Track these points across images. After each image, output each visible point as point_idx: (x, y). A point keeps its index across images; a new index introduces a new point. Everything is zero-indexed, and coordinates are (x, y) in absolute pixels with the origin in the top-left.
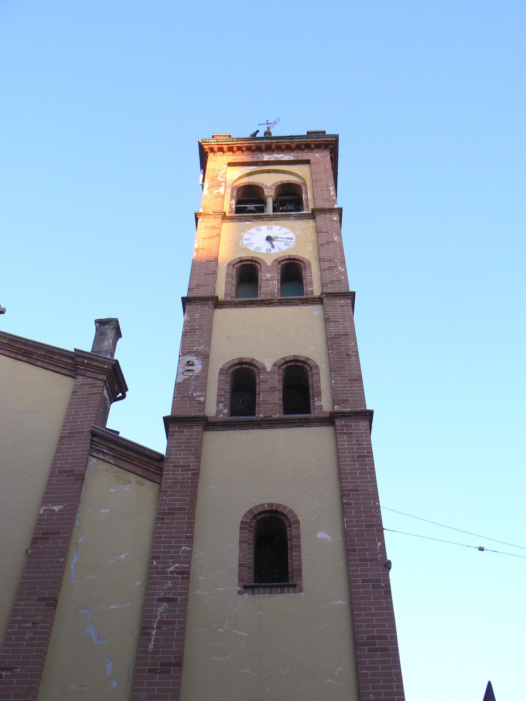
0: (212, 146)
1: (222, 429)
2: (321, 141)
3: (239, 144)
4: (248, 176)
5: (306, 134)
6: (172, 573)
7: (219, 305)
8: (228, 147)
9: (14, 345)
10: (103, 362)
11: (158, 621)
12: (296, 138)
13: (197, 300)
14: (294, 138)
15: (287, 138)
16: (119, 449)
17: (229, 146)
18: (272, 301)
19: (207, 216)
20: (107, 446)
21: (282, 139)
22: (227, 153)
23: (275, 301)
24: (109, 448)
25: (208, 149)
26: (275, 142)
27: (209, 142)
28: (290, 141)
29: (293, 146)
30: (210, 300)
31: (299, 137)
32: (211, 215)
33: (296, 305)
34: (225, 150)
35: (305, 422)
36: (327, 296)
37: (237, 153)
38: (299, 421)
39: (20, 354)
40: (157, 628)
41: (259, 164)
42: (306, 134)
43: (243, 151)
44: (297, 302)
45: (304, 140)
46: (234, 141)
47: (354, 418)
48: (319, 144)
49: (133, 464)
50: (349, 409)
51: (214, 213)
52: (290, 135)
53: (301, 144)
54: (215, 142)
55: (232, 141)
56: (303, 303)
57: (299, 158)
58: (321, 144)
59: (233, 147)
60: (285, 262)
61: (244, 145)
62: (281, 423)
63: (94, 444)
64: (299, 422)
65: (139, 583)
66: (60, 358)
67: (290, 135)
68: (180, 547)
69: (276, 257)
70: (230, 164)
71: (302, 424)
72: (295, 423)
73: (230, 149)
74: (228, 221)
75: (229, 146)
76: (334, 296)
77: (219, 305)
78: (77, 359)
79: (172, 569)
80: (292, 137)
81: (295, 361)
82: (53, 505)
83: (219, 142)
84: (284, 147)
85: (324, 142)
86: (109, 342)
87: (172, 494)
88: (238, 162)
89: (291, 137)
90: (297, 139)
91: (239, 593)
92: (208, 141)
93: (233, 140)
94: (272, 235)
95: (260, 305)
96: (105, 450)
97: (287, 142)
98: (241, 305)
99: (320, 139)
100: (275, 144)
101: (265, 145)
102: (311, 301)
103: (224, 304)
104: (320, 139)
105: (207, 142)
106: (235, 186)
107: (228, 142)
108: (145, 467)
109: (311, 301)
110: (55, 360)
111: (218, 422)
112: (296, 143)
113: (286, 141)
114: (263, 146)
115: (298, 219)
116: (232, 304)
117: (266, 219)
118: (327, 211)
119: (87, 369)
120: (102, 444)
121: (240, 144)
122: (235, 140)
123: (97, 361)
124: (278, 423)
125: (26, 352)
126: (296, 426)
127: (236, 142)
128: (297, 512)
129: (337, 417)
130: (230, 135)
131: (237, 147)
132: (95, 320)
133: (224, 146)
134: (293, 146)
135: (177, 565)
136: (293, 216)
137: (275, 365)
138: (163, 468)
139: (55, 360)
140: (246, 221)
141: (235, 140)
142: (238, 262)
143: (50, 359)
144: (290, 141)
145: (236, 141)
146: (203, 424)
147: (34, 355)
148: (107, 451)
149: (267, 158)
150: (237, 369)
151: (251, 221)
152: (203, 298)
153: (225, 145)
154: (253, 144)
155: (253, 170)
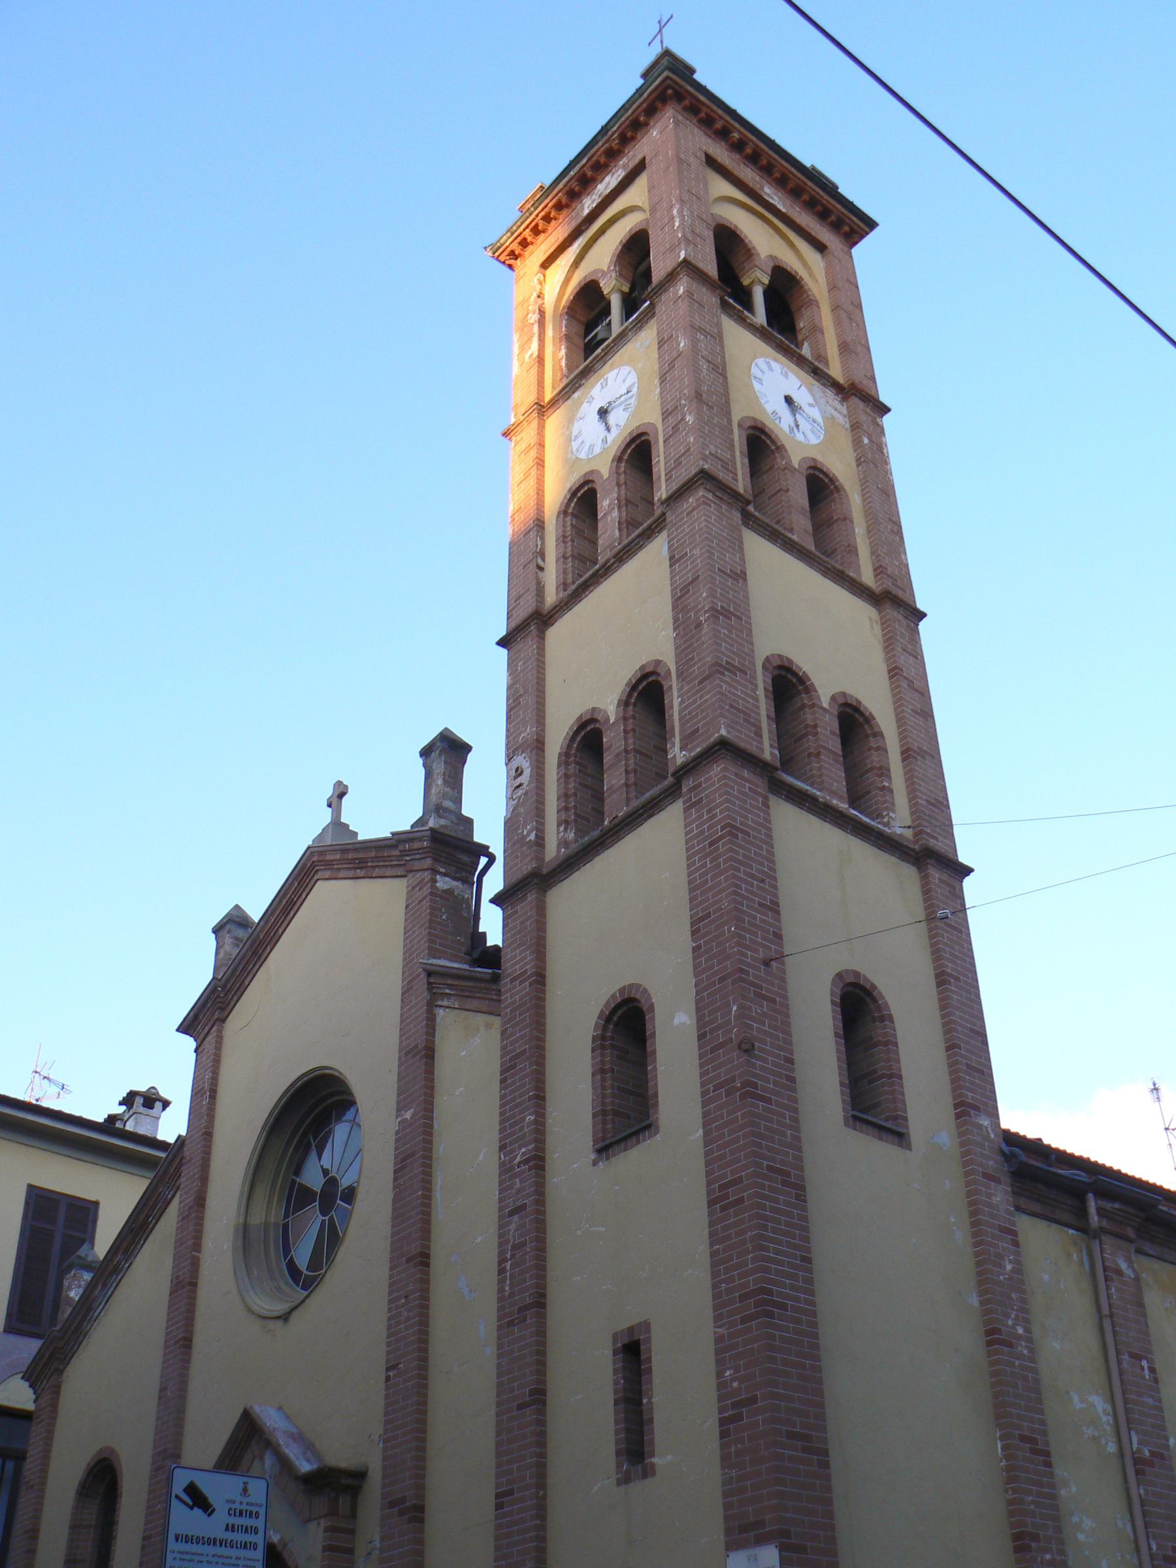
0: (509, 249)
1: (566, 875)
2: (649, 95)
4: (576, 268)
5: (641, 81)
6: (519, 1165)
7: (549, 618)
8: (531, 230)
11: (512, 1246)
13: (515, 635)
14: (609, 127)
15: (598, 138)
17: (530, 227)
18: (609, 564)
19: (518, 428)
21: (594, 146)
22: (526, 253)
23: (612, 561)
24: (450, 986)
25: (508, 258)
26: (587, 162)
27: (502, 245)
28: (605, 139)
29: (615, 144)
30: (529, 624)
31: (613, 122)
32: (522, 422)
33: (641, 548)
34: (577, 189)
35: (654, 806)
36: (668, 505)
37: (550, 229)
38: (645, 809)
40: (513, 1256)
41: (583, 228)
42: (641, 81)
44: (639, 542)
45: (623, 119)
46: (533, 212)
47: (705, 765)
48: (649, 106)
49: (475, 998)
50: (698, 750)
51: (523, 415)
52: (600, 128)
53: (623, 131)
54: (509, 238)
55: (531, 214)
56: (649, 538)
57: (631, 165)
58: (654, 101)
59: (537, 225)
60: (633, 446)
61: (549, 206)
62: (628, 824)
63: (434, 987)
64: (645, 812)
67: (598, 128)
68: (523, 1119)
69: (613, 452)
71: (651, 812)
73: (536, 231)
74: (551, 410)
75: (530, 227)
76: (678, 496)
77: (549, 618)
79: (518, 1159)
80: (640, 92)
83: (515, 231)
84: (603, 160)
85: (654, 95)
86: (437, 785)
88: (552, 253)
89: (604, 130)
90: (613, 126)
91: (595, 1163)
92: (499, 244)
93: (530, 211)
94: (603, 404)
95: (597, 583)
97: (602, 146)
98: (574, 600)
99: (645, 95)
100: (588, 165)
101: (576, 181)
102: (656, 527)
103: (554, 614)
104: (645, 95)
105: (499, 248)
106: (564, 306)
107: (527, 218)
109: (656, 527)
110: (386, 859)
111: (555, 870)
112: (616, 135)
113: (600, 144)
114: (574, 184)
115: (641, 328)
116: (562, 607)
117: (597, 365)
118: (667, 282)
121: (542, 210)
124: (623, 828)
126: (646, 820)
127: (537, 212)
128: (651, 991)
130: (541, 187)
131: (542, 219)
132: (446, 729)
133: (524, 233)
134: (615, 144)
135: (523, 1150)
136: (630, 330)
137: (625, 703)
138: (500, 991)
139: (386, 859)
140: (573, 393)
141: (532, 209)
142: (570, 500)
144: (605, 139)
145: (535, 209)
146: (536, 884)
147: (368, 862)
150: (583, 738)
151: (580, 386)
152: (519, 626)
153: (524, 230)
154: (560, 195)
155: (578, 251)
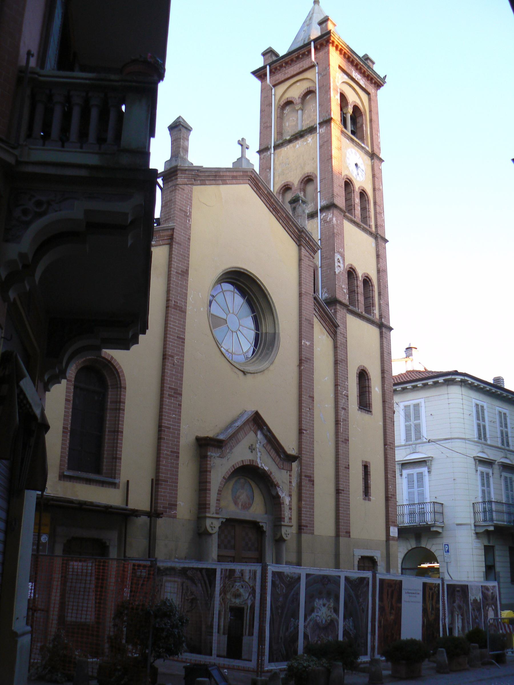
2: (379, 81)
3: (346, 50)
9: (270, 198)
10: (315, 245)
12: (371, 69)
14: (370, 69)
16: (323, 313)
20: (319, 309)
39: (271, 207)
41: (349, 77)
43: (341, 53)
65: (332, 395)
66: (292, 225)
70: (340, 67)
72: (370, 322)
78: (303, 234)
81: (370, 280)
82: (306, 341)
87: (157, 227)
92: (335, 34)
96: (317, 310)
108: (330, 327)
119: (306, 244)
120: (317, 306)
122: (346, 46)
123: (312, 242)
125: (276, 208)
129: (384, 327)
143: (287, 223)
144: (367, 69)
148: (317, 311)
149: (333, 52)
153: (341, 45)
